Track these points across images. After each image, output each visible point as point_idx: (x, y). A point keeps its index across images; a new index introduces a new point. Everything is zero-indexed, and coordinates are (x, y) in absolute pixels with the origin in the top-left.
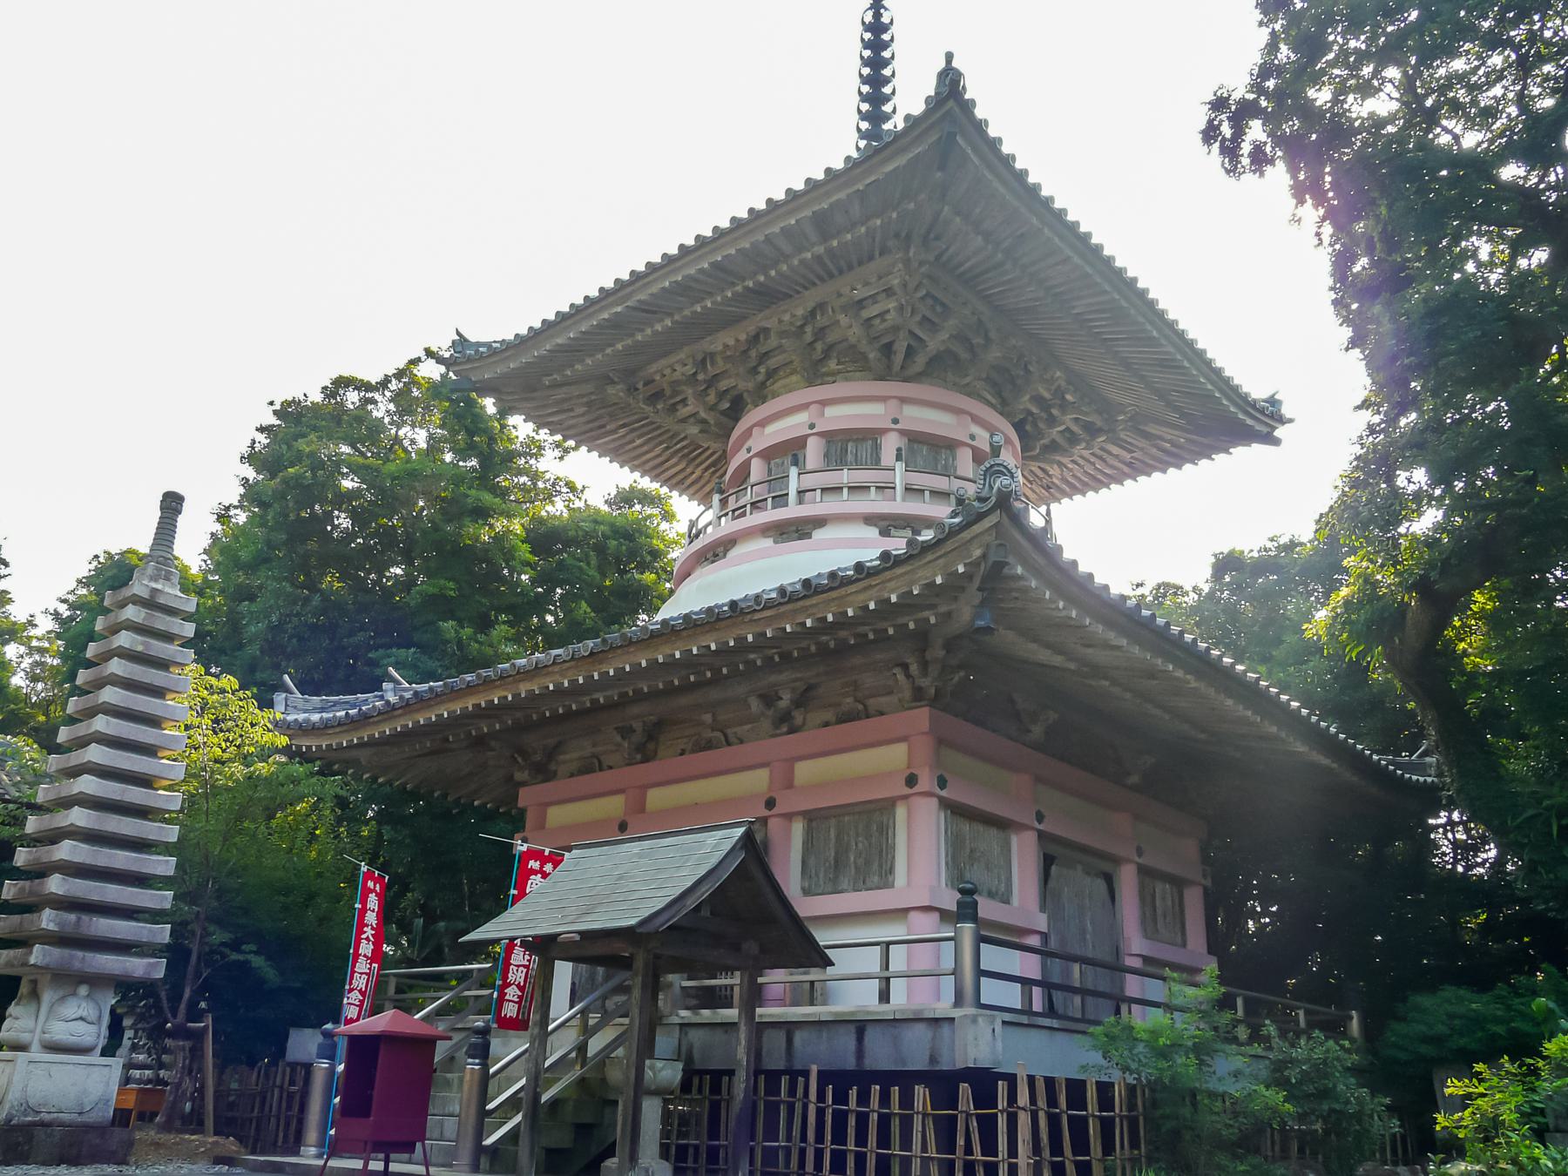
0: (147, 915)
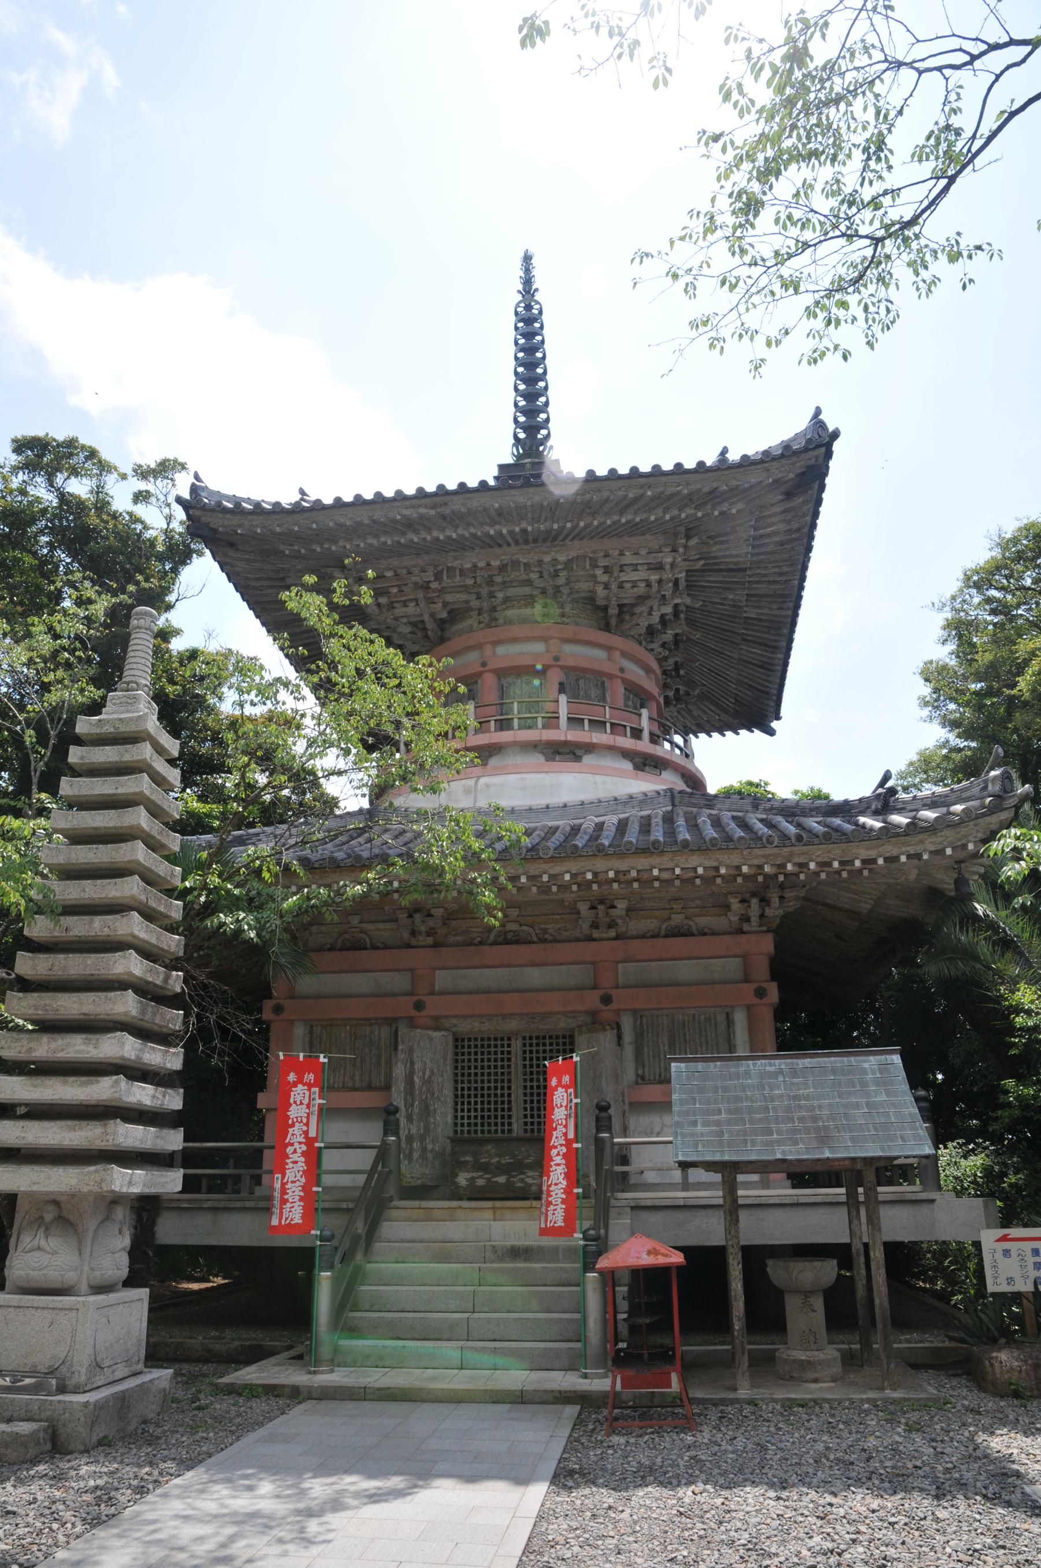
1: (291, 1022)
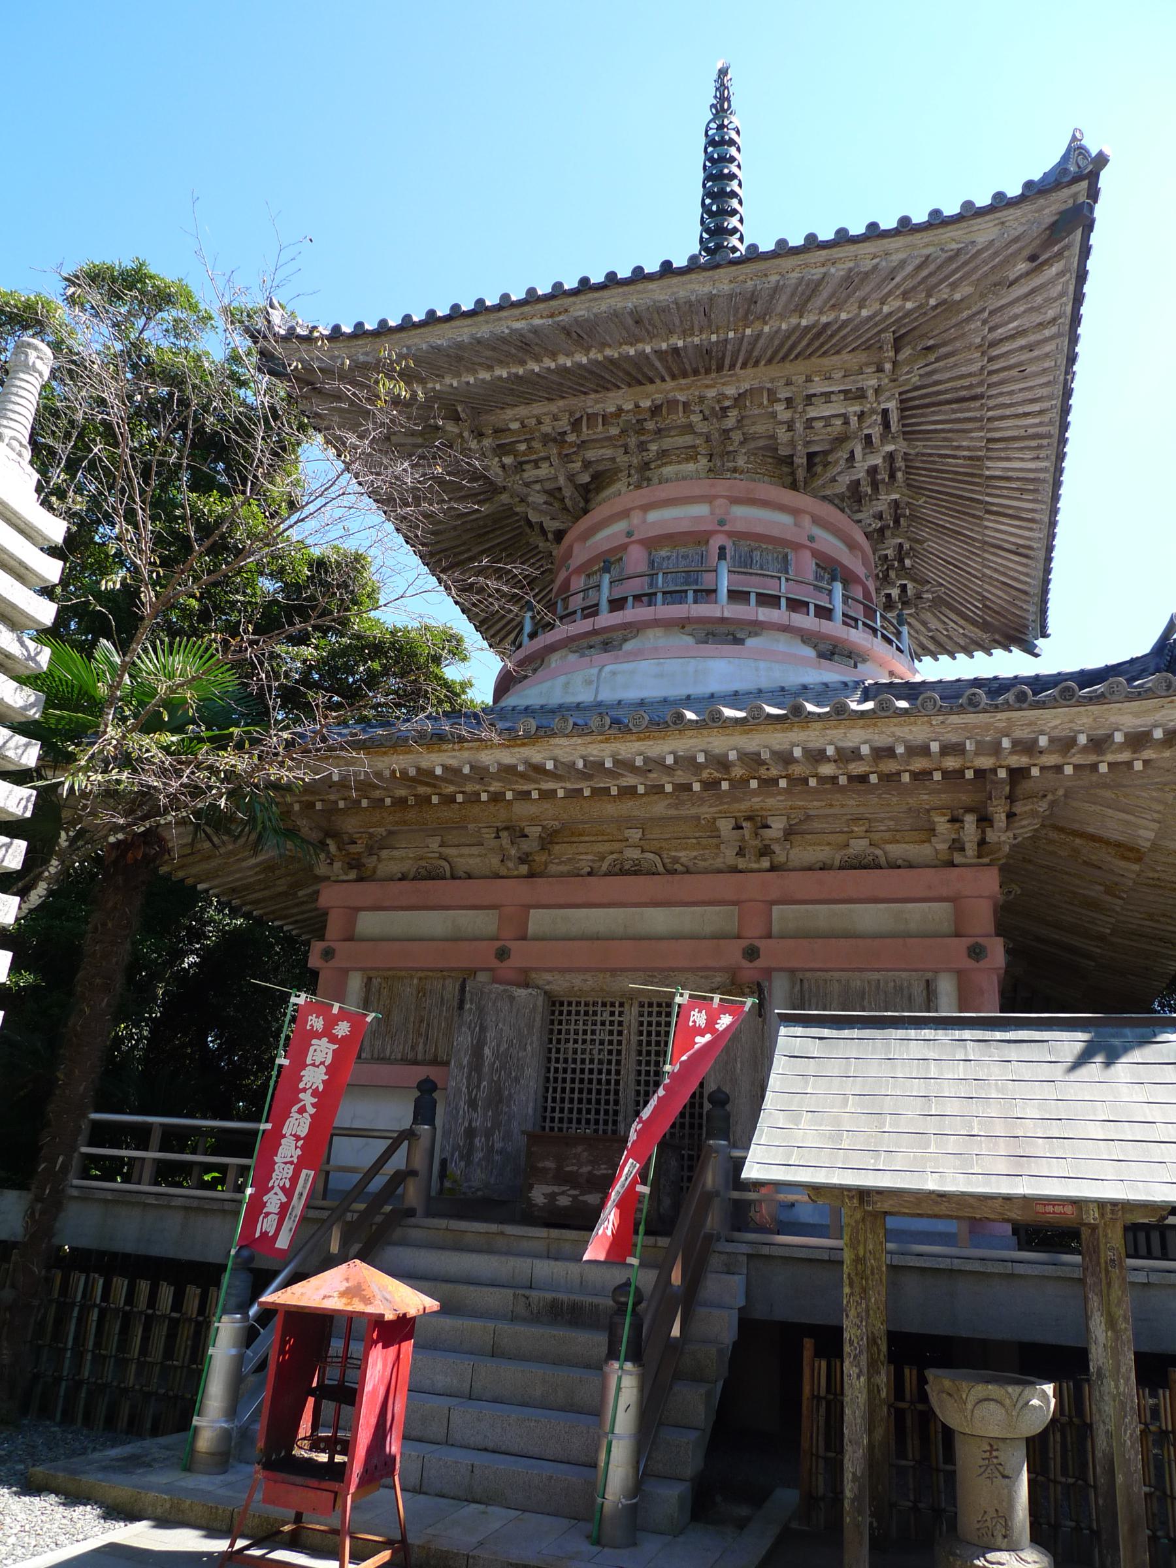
0: (667, 1202)
1: (345, 972)
